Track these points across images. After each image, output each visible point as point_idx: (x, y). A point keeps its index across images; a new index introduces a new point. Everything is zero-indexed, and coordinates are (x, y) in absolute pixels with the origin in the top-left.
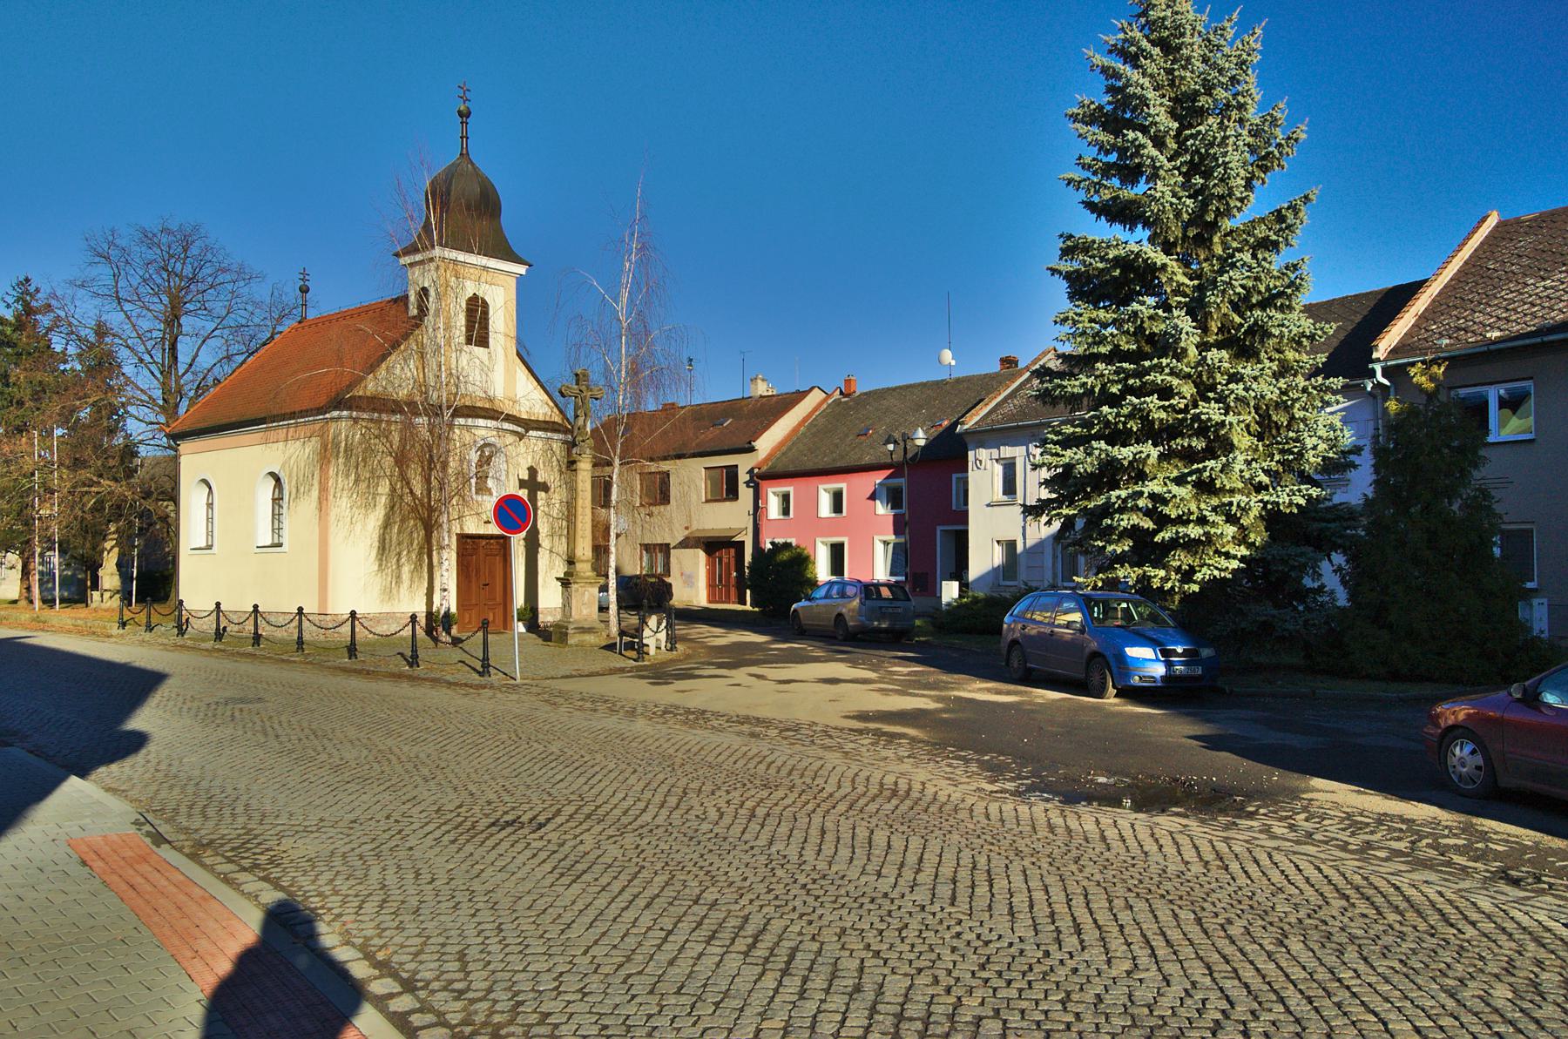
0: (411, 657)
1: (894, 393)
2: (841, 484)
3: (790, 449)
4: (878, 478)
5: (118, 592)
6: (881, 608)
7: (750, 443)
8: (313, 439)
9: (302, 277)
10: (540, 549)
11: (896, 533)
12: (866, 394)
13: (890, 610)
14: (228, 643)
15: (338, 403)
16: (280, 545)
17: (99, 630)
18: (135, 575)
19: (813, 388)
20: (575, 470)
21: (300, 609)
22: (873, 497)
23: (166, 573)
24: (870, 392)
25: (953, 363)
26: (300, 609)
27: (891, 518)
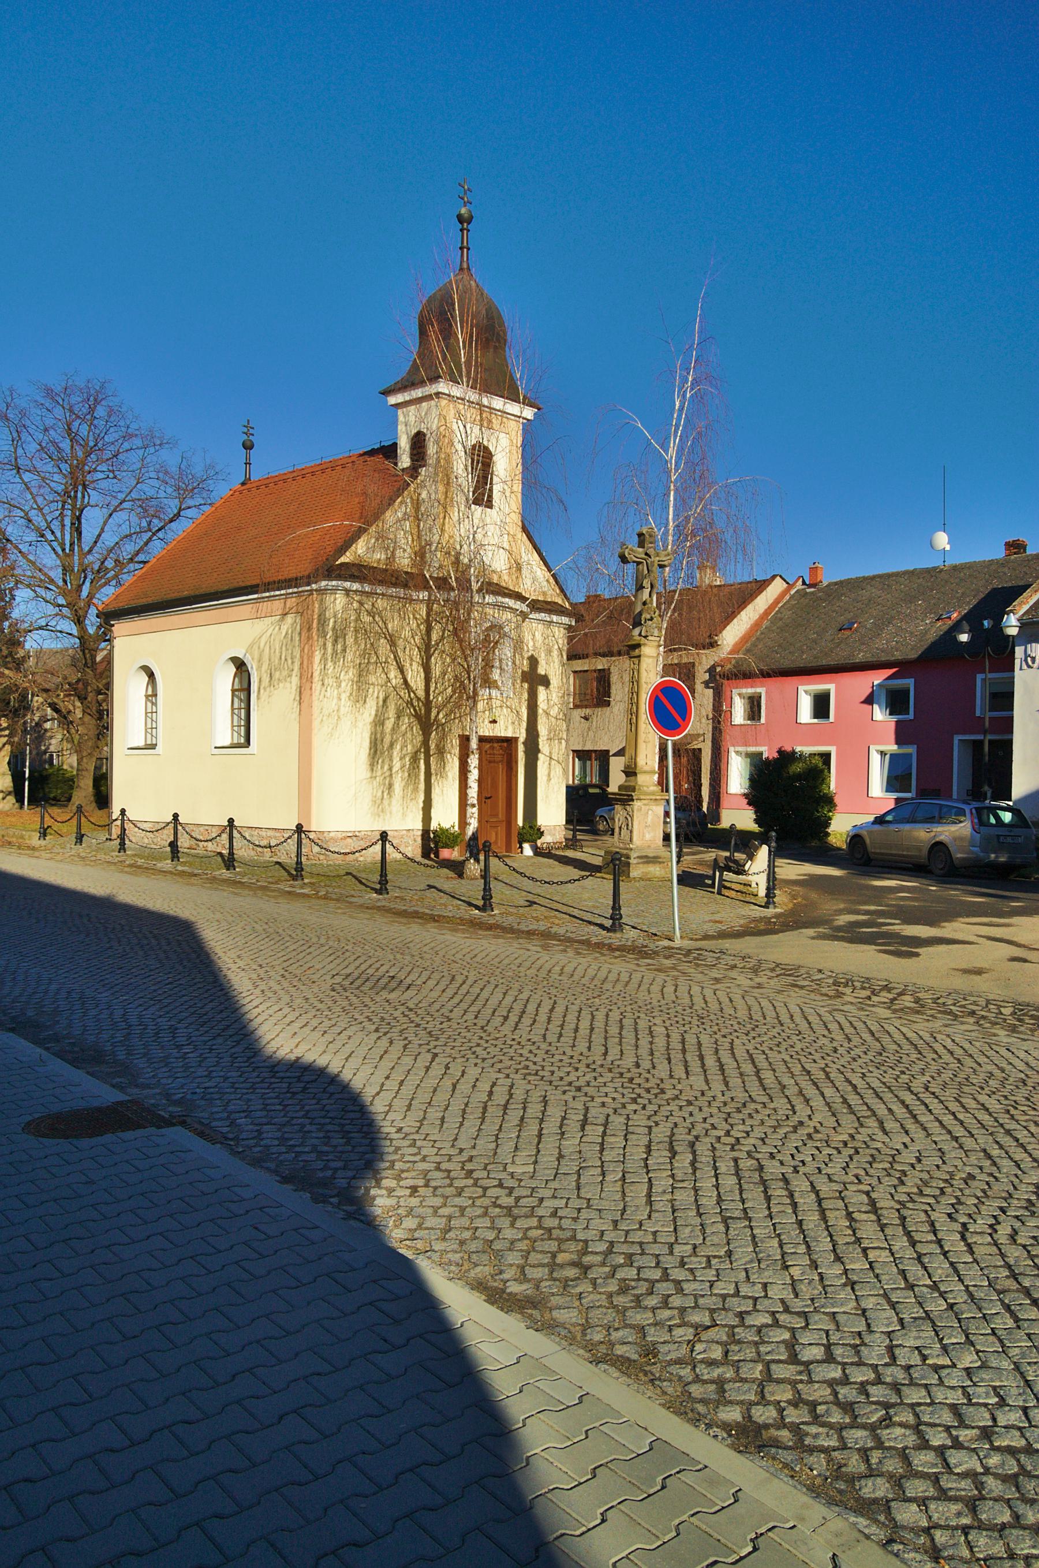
0: (296, 870)
1: (873, 582)
2: (828, 685)
3: (754, 645)
4: (878, 678)
5: (9, 793)
6: (998, 836)
7: (710, 636)
8: (289, 619)
9: (245, 430)
10: (540, 755)
11: (899, 741)
12: (836, 583)
13: (1009, 840)
14: (184, 864)
15: (334, 571)
16: (153, 747)
17: (14, 840)
18: (27, 775)
19: (774, 577)
20: (639, 656)
21: (231, 821)
22: (869, 700)
23: (45, 773)
24: (841, 582)
25: (948, 548)
26: (231, 821)
27: (893, 725)
